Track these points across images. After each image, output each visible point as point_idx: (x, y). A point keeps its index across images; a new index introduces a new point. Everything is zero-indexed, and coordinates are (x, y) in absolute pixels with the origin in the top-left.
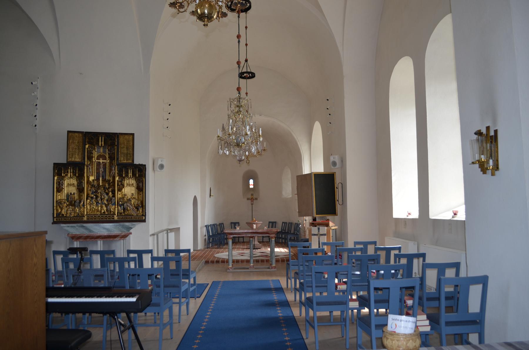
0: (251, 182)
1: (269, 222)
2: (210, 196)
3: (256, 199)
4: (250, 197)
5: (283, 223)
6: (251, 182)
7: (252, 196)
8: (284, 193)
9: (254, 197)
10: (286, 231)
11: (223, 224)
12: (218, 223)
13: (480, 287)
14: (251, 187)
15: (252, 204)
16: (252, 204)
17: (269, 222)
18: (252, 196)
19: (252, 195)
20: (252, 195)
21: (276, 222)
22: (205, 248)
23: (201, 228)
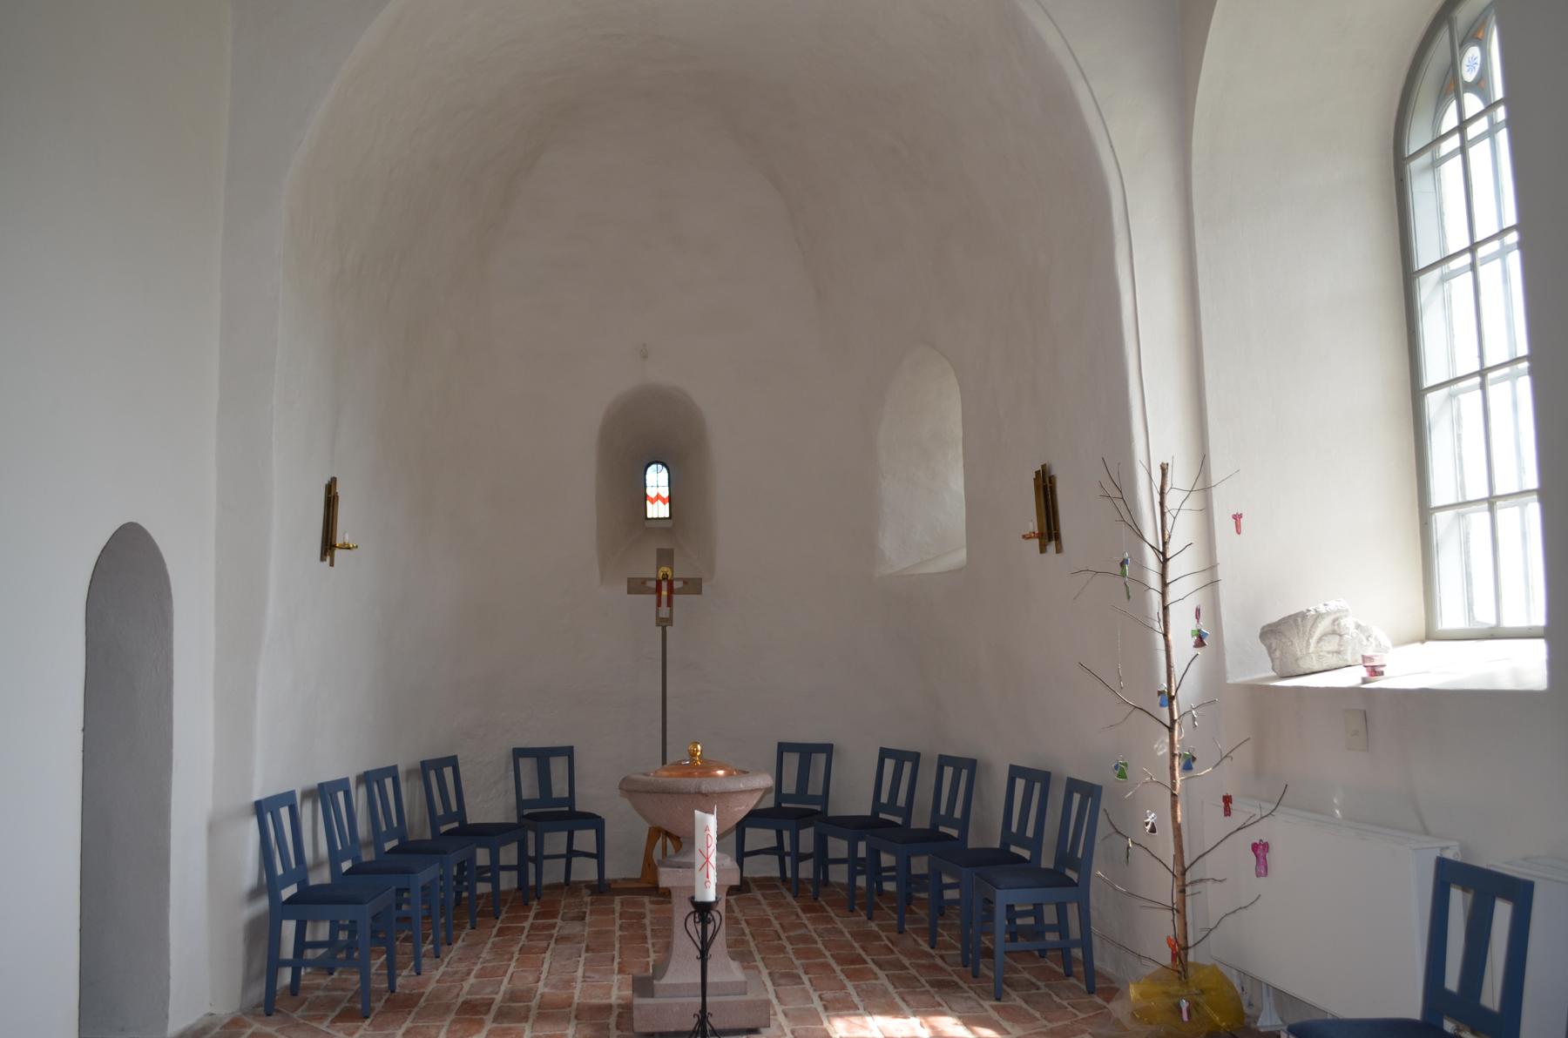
0: (657, 480)
1: (783, 748)
2: (328, 546)
3: (694, 586)
4: (649, 569)
5: (884, 753)
6: (657, 480)
7: (666, 570)
8: (888, 543)
9: (680, 571)
10: (1047, 862)
11: (453, 762)
12: (405, 760)
13: (822, 757)
14: (658, 510)
15: (664, 623)
16: (664, 623)
17: (783, 748)
18: (666, 570)
19: (665, 557)
20: (665, 557)
21: (828, 749)
22: (251, 1011)
23: (213, 828)
